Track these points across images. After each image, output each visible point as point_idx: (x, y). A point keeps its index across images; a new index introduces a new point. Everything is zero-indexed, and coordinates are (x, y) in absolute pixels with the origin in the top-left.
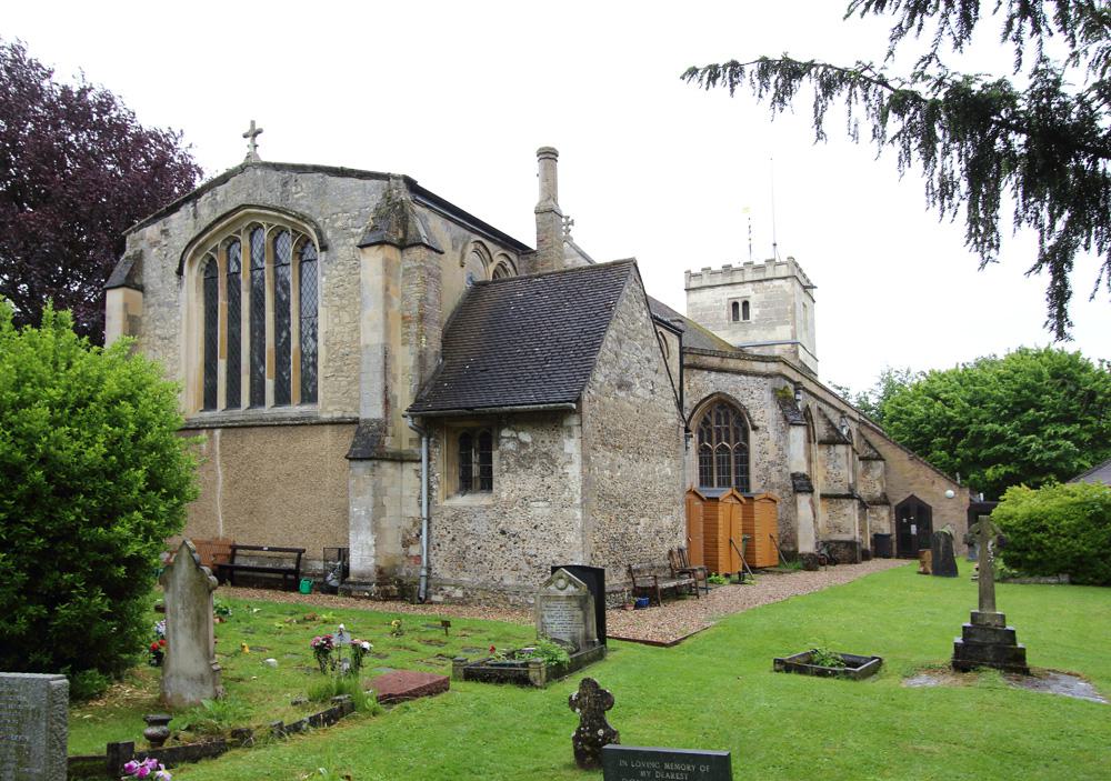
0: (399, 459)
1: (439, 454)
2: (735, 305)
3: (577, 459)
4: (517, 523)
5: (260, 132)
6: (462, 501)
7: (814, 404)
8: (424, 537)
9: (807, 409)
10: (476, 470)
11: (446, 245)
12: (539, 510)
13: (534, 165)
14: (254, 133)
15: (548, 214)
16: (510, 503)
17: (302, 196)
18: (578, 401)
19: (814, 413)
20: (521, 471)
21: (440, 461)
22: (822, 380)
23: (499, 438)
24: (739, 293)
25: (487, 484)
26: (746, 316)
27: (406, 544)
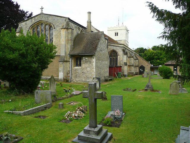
0: (66, 61)
1: (73, 62)
2: (116, 33)
3: (95, 62)
4: (85, 71)
5: (43, 8)
6: (76, 68)
7: (128, 51)
8: (70, 73)
9: (127, 52)
10: (78, 63)
11: (74, 28)
12: (88, 69)
13: (87, 15)
14: (42, 8)
15: (89, 22)
16: (84, 68)
17: (50, 20)
18: (95, 53)
19: (128, 53)
20: (86, 63)
21: (72, 62)
22: (129, 47)
23: (82, 59)
24: (116, 31)
25: (80, 65)
26: (117, 35)
27: (67, 74)
